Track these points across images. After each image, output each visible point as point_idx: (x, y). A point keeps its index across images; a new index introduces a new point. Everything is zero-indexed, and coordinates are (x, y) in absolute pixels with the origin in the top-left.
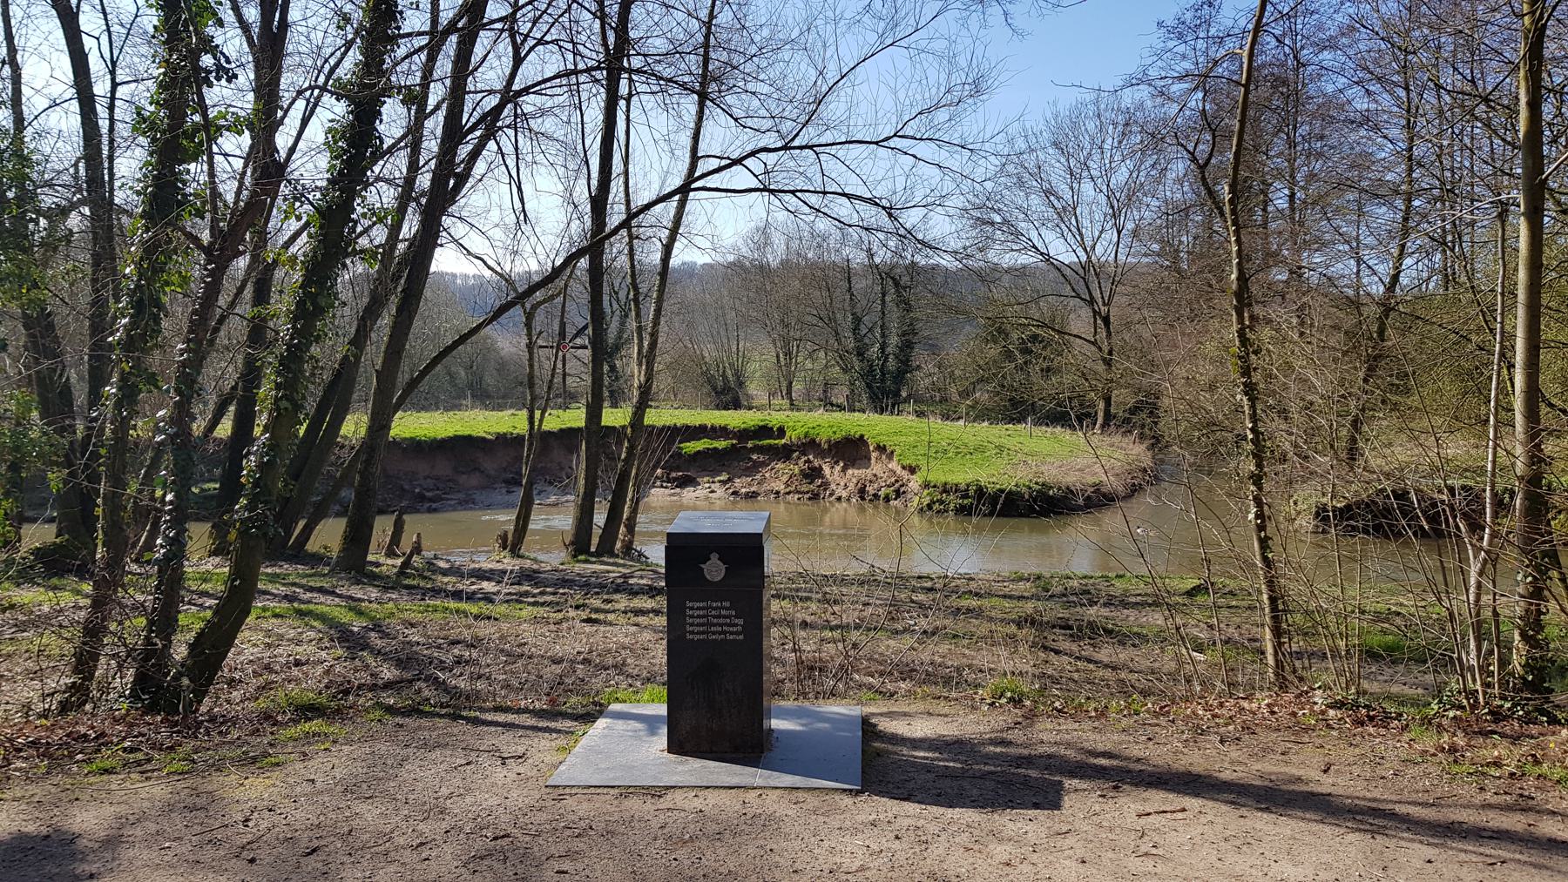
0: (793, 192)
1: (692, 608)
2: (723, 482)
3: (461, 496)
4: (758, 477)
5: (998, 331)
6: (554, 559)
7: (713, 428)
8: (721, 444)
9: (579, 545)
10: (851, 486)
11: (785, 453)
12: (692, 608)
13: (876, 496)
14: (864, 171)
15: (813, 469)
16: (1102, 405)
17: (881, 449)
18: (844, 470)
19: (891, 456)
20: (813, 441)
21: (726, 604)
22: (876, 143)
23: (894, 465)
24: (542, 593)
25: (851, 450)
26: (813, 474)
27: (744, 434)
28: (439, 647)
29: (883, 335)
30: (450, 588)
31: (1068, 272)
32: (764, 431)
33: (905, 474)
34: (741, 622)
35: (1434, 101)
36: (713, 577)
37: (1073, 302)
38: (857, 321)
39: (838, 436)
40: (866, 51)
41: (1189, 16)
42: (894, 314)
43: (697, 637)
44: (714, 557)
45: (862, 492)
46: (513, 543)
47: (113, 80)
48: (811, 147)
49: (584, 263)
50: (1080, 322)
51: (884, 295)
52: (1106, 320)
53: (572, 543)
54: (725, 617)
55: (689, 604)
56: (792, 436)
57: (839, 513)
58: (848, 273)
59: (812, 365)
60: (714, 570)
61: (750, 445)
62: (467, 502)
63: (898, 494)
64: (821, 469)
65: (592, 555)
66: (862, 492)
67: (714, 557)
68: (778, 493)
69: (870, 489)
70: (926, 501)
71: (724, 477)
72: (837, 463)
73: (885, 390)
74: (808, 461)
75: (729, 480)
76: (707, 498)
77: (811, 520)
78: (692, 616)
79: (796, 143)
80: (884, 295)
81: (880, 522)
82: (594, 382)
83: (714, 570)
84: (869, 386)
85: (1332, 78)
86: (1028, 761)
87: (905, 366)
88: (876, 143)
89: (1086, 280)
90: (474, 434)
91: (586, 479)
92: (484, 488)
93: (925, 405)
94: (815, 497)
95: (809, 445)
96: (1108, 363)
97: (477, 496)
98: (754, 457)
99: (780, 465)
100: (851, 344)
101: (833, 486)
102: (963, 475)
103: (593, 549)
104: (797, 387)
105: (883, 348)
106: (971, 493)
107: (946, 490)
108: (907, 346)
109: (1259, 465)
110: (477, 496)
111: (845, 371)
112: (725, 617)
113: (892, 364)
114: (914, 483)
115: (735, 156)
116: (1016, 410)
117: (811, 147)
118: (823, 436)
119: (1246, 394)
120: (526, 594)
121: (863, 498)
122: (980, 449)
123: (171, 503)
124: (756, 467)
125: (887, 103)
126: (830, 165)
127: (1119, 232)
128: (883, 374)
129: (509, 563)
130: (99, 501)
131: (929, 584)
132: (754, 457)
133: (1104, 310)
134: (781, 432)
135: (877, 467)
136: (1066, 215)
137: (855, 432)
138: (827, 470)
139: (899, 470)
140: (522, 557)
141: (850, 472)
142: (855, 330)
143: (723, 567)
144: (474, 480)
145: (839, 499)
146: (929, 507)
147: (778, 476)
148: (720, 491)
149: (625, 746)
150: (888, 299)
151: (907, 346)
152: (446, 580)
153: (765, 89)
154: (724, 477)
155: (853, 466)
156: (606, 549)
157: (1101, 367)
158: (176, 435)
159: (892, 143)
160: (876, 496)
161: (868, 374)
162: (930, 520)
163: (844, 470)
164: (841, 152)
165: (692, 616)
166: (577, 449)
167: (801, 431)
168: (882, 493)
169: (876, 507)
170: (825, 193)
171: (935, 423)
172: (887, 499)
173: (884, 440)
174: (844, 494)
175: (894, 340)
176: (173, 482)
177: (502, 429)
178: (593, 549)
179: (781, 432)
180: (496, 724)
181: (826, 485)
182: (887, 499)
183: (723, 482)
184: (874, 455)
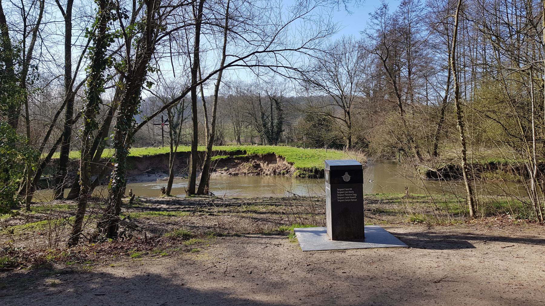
0: (269, 66)
1: (339, 191)
2: (226, 170)
3: (131, 178)
4: (238, 168)
5: (310, 118)
6: (183, 196)
7: (221, 152)
8: (224, 157)
9: (191, 191)
10: (271, 170)
11: (247, 159)
12: (339, 191)
13: (280, 173)
14: (290, 60)
15: (257, 165)
16: (348, 141)
17: (280, 157)
18: (268, 164)
19: (284, 159)
20: (256, 155)
21: (351, 189)
22: (295, 50)
23: (285, 162)
24: (185, 207)
25: (270, 158)
26: (257, 166)
27: (232, 153)
28: (163, 225)
29: (272, 119)
30: (150, 207)
31: (337, 98)
32: (239, 152)
33: (289, 165)
34: (356, 195)
35: (535, 31)
36: (347, 180)
37: (336, 107)
38: (263, 114)
39: (265, 153)
40: (290, 19)
41: (379, 11)
42: (275, 112)
43: (341, 201)
44: (346, 173)
45: (275, 172)
46: (167, 191)
47: (25, 24)
48: (273, 51)
49: (190, 93)
50: (339, 113)
51: (272, 106)
52: (348, 113)
53: (188, 191)
54: (350, 193)
55: (338, 190)
56: (249, 153)
57: (267, 179)
58: (259, 99)
59: (247, 130)
60: (347, 177)
61: (234, 157)
62: (133, 180)
63: (287, 172)
64: (259, 164)
65: (196, 194)
66: (275, 172)
67: (346, 173)
68: (245, 173)
69: (277, 171)
70: (298, 174)
71: (226, 168)
72: (265, 162)
73: (274, 137)
74: (255, 162)
75: (228, 169)
76: (221, 176)
77: (257, 182)
78: (339, 194)
79: (268, 49)
80: (272, 106)
81: (280, 181)
82: (194, 134)
83: (347, 177)
84: (268, 137)
85: (422, 33)
86: (436, 237)
87: (280, 131)
88: (295, 50)
89: (343, 101)
90: (135, 155)
91: (193, 168)
92: (139, 175)
93: (290, 141)
94: (258, 174)
95: (255, 156)
96: (349, 127)
97: (137, 178)
98: (236, 161)
99: (245, 164)
100: (260, 122)
101: (264, 170)
102: (310, 165)
103: (196, 191)
104: (242, 139)
105: (272, 123)
106: (314, 171)
107: (304, 170)
108: (280, 123)
109: (465, 148)
110: (137, 178)
111: (259, 132)
112: (350, 193)
113: (275, 129)
114: (293, 168)
115: (241, 57)
116: (319, 144)
117: (273, 51)
118: (260, 153)
119: (460, 125)
120: (179, 208)
121: (275, 174)
122: (313, 156)
123: (117, 167)
124: (236, 165)
125: (298, 37)
126: (279, 57)
127: (352, 84)
128: (272, 133)
129: (167, 198)
130: (80, 169)
131: (316, 199)
132: (236, 161)
133: (347, 109)
134: (245, 152)
135: (279, 163)
136: (335, 79)
137: (271, 151)
138: (262, 165)
139: (287, 164)
140: (171, 196)
141: (270, 165)
142: (263, 117)
143: (350, 177)
144: (135, 172)
145: (267, 174)
146: (299, 176)
147: (245, 167)
148: (225, 174)
149: (316, 240)
150: (273, 107)
151: (280, 123)
152: (147, 204)
153: (258, 31)
154: (226, 168)
155: (271, 163)
156: (201, 192)
157: (347, 129)
158: (118, 143)
159: (300, 50)
160: (280, 173)
161: (267, 133)
162: (300, 180)
163: (268, 164)
164: (282, 53)
165: (339, 194)
166: (189, 157)
167: (252, 152)
168: (282, 172)
169: (280, 177)
170: (277, 66)
171: (295, 148)
172: (284, 174)
173: (281, 154)
174: (268, 173)
175: (276, 121)
176: (118, 160)
177: (145, 154)
178: (196, 191)
179: (245, 152)
180: (253, 237)
181: (262, 170)
182: (284, 174)
183: (226, 170)
184: (278, 159)
